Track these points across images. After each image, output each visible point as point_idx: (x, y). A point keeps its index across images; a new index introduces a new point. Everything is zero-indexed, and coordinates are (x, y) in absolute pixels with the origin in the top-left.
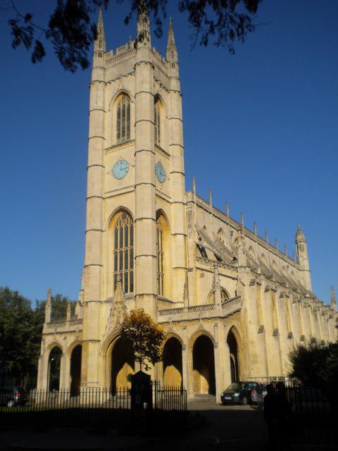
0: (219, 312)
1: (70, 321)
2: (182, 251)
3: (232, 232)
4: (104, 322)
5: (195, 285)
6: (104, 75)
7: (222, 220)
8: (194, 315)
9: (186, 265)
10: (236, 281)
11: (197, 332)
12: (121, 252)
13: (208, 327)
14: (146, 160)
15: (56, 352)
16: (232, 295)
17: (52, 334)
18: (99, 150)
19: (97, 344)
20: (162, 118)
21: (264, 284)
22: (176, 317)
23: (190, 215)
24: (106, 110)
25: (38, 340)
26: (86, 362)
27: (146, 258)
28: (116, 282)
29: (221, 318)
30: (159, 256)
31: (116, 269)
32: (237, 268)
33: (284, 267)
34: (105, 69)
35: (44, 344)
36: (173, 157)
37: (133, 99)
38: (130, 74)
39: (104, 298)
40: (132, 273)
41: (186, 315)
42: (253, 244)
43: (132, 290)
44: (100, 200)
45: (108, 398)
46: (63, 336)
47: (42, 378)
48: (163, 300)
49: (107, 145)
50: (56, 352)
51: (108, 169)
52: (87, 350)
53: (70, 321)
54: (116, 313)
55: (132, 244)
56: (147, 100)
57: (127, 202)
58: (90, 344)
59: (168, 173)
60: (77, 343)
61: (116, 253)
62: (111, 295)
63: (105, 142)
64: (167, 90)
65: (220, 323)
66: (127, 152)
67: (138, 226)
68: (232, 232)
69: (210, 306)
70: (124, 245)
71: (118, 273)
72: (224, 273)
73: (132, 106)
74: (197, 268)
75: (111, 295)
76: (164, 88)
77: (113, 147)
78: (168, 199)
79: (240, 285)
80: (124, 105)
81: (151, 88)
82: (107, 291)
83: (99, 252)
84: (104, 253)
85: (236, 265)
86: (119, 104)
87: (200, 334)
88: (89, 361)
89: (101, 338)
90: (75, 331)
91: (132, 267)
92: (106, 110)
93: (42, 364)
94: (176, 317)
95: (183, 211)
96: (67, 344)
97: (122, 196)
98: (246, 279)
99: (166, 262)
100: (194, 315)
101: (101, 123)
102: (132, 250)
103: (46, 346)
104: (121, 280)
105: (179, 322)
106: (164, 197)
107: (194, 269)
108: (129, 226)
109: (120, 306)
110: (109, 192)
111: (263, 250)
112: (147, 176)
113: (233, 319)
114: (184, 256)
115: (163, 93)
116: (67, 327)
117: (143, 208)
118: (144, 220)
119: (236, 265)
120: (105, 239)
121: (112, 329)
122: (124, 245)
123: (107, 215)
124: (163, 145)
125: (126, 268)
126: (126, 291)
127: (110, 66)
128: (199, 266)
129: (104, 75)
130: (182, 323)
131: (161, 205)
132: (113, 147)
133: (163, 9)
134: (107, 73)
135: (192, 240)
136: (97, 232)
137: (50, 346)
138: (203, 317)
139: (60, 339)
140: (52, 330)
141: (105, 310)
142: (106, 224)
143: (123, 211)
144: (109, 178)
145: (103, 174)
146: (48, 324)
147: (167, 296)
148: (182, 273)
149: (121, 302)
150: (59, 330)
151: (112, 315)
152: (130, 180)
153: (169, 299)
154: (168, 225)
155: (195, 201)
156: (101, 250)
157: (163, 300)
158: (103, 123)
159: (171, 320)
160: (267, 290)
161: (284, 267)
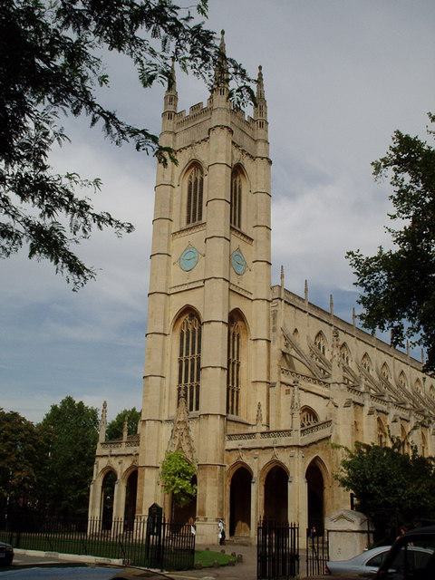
0: (297, 438)
2: (264, 360)
4: (164, 446)
5: (279, 404)
6: (175, 141)
8: (267, 442)
9: (269, 378)
10: (327, 401)
11: (270, 463)
13: (283, 457)
14: (218, 248)
15: (110, 478)
16: (322, 418)
17: (107, 456)
18: (164, 234)
19: (155, 472)
20: (244, 192)
21: (368, 404)
22: (247, 443)
25: (91, 461)
26: (142, 491)
28: (179, 397)
29: (299, 446)
30: (232, 368)
31: (180, 382)
33: (418, 380)
37: (205, 172)
38: (205, 140)
39: (165, 417)
40: (198, 387)
41: (260, 442)
42: (369, 350)
43: (197, 409)
44: (163, 296)
46: (120, 459)
48: (236, 422)
49: (175, 228)
50: (110, 478)
51: (174, 257)
52: (143, 477)
55: (199, 352)
57: (192, 299)
58: (147, 470)
59: (249, 262)
60: (133, 469)
62: (173, 413)
63: (173, 224)
64: (252, 157)
65: (298, 454)
66: (196, 237)
69: (287, 432)
70: (194, 407)
71: (183, 387)
73: (205, 179)
75: (173, 413)
76: (248, 154)
78: (249, 296)
79: (331, 406)
81: (227, 159)
82: (169, 408)
83: (160, 360)
84: (167, 361)
85: (329, 381)
86: (191, 177)
87: (239, 466)
88: (145, 492)
89: (160, 465)
90: (131, 455)
91: (198, 380)
92: (175, 185)
94: (247, 443)
96: (121, 468)
98: (341, 396)
99: (243, 375)
100: (267, 442)
102: (199, 358)
104: (186, 395)
105: (250, 449)
106: (246, 295)
109: (183, 427)
111: (385, 358)
112: (218, 269)
113: (317, 448)
114: (266, 368)
115: (247, 163)
116: (123, 449)
117: (214, 309)
119: (329, 381)
120: (168, 345)
122: (194, 407)
123: (172, 315)
124: (243, 229)
125: (192, 380)
126: (191, 410)
128: (284, 380)
129: (175, 141)
130: (252, 451)
131: (237, 303)
133: (249, 80)
135: (278, 346)
139: (115, 463)
140: (106, 452)
141: (166, 430)
142: (169, 329)
143: (189, 311)
144: (175, 270)
147: (242, 417)
148: (264, 387)
150: (115, 452)
151: (173, 437)
152: (198, 274)
154: (246, 328)
156: (163, 358)
157: (236, 422)
159: (241, 447)
160: (370, 413)
161: (418, 380)
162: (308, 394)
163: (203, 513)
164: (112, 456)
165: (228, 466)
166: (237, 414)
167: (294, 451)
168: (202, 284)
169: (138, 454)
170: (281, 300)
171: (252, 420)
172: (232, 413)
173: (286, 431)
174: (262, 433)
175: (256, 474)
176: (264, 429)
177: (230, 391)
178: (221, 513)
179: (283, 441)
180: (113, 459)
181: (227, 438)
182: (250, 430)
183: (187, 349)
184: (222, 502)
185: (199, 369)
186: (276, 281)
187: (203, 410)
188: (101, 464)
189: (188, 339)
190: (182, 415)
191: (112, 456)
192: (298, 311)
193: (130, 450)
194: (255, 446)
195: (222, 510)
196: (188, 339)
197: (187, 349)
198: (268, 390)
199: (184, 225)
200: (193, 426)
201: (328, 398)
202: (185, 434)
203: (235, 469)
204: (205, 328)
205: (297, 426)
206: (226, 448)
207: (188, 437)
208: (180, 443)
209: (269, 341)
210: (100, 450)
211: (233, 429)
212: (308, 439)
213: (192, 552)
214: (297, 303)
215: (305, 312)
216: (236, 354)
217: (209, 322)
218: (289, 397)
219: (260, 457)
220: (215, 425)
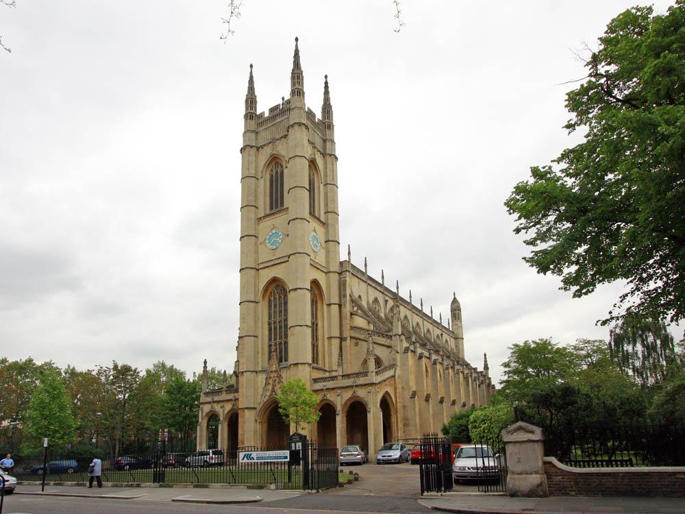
3: (387, 301)
10: (389, 350)
22: (330, 384)
28: (270, 352)
35: (202, 411)
43: (286, 360)
52: (243, 416)
53: (226, 391)
68: (387, 301)
77: (266, 216)
80: (277, 171)
85: (390, 334)
86: (272, 171)
87: (323, 403)
93: (201, 430)
105: (333, 389)
110: (262, 263)
118: (298, 290)
121: (267, 397)
123: (262, 286)
126: (281, 361)
132: (266, 216)
136: (251, 304)
138: (357, 384)
140: (209, 399)
149: (276, 371)
150: (216, 398)
164: (214, 402)
168: (286, 259)
175: (339, 408)
180: (215, 405)
182: (334, 374)
190: (274, 366)
191: (214, 402)
193: (231, 396)
197: (280, 333)
199: (268, 212)
202: (277, 380)
208: (273, 388)
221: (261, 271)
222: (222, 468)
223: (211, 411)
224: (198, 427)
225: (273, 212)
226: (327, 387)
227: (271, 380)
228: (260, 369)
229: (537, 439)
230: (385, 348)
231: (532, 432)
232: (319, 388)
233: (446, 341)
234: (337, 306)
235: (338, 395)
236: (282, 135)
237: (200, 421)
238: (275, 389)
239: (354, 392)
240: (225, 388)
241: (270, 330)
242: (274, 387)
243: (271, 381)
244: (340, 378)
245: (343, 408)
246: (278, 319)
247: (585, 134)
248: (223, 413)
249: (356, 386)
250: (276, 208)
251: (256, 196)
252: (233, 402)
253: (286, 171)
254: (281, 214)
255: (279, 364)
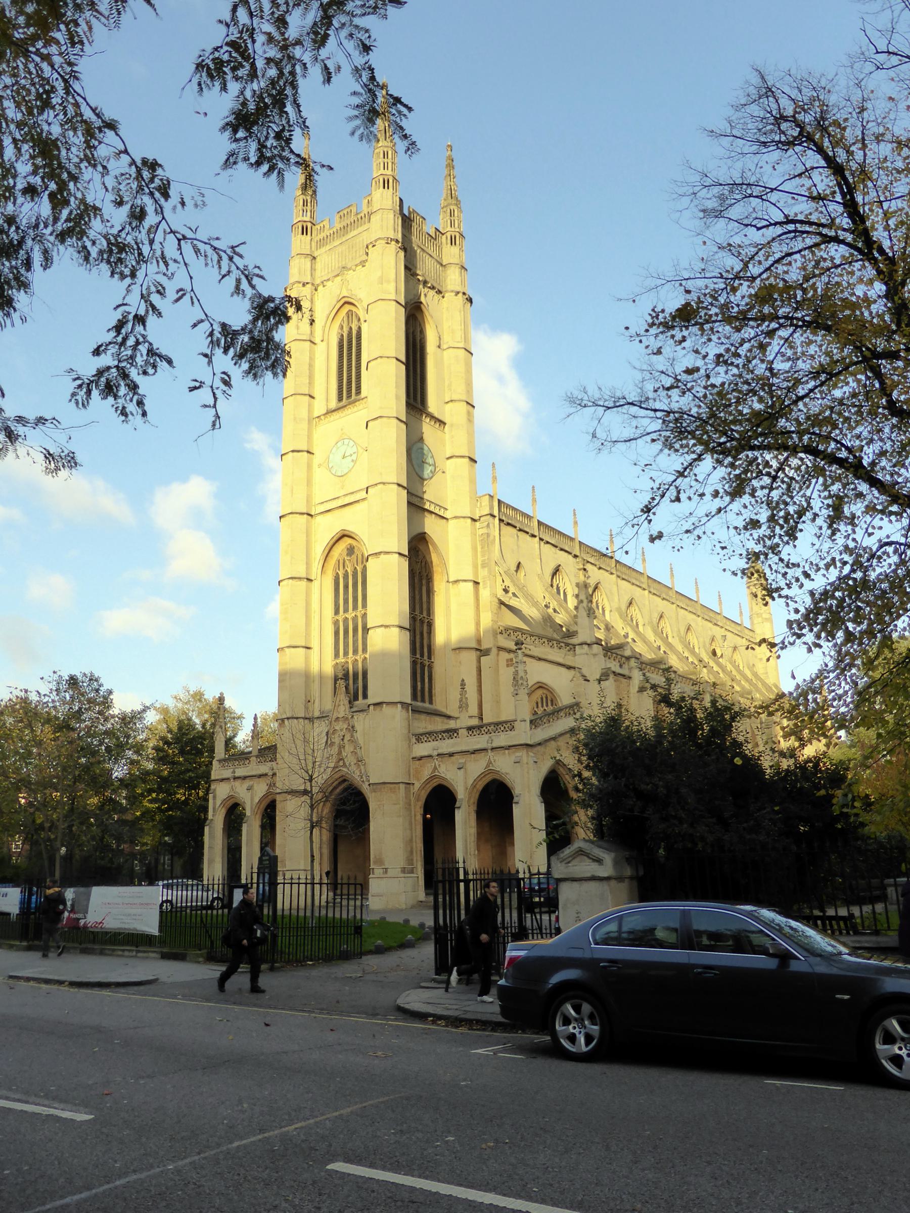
0: (523, 734)
1: (257, 757)
6: (313, 269)
7: (562, 550)
8: (480, 741)
10: (572, 672)
12: (346, 620)
22: (446, 746)
23: (487, 539)
24: (317, 340)
27: (387, 630)
32: (574, 646)
34: (314, 258)
35: (214, 798)
36: (452, 425)
43: (365, 696)
45: (324, 897)
46: (247, 783)
47: (211, 862)
49: (319, 407)
53: (257, 757)
54: (337, 740)
55: (364, 605)
56: (146, 242)
60: (270, 798)
61: (336, 623)
66: (355, 415)
67: (373, 566)
69: (507, 725)
72: (550, 657)
74: (500, 649)
76: (433, 288)
77: (329, 412)
80: (351, 328)
85: (574, 641)
86: (342, 327)
87: (488, 779)
93: (212, 836)
95: (474, 534)
97: (347, 508)
101: (307, 367)
102: (364, 616)
103: (218, 802)
105: (451, 755)
107: (463, 732)
108: (359, 569)
118: (382, 556)
119: (574, 641)
123: (318, 550)
126: (356, 698)
127: (323, 250)
129: (313, 269)
130: (456, 757)
132: (329, 412)
134: (319, 265)
136: (299, 583)
137: (224, 801)
138: (495, 745)
140: (227, 773)
145: (309, 466)
146: (220, 761)
148: (473, 655)
149: (345, 719)
150: (240, 772)
153: (444, 710)
155: (496, 513)
157: (428, 713)
158: (311, 366)
160: (642, 690)
162: (542, 663)
163: (380, 862)
164: (235, 778)
165: (417, 785)
166: (431, 702)
167: (522, 754)
168: (363, 494)
169: (274, 774)
170: (494, 517)
171: (452, 710)
172: (423, 701)
173: (506, 722)
174: (470, 729)
175: (461, 794)
176: (475, 722)
177: (418, 666)
178: (410, 861)
179: (502, 739)
180: (237, 784)
181: (414, 740)
182: (452, 724)
183: (346, 601)
184: (411, 840)
185: (366, 630)
186: (485, 487)
187: (371, 699)
188: (220, 793)
189: (346, 587)
190: (342, 708)
191: (235, 778)
192: (521, 534)
193: (264, 768)
194: (459, 749)
195: (411, 852)
196: (346, 587)
197: (346, 601)
198: (479, 661)
199: (333, 403)
200: (361, 722)
201: (574, 668)
202: (347, 737)
203: (429, 788)
204: (372, 564)
205: (526, 713)
206: (414, 756)
207: (353, 741)
208: (340, 753)
209: (476, 583)
210: (217, 771)
211: (425, 724)
212: (541, 734)
213: (358, 930)
214: (519, 520)
215: (533, 536)
216: (425, 606)
217: (377, 554)
218: (512, 669)
219: (255, 787)
220: (396, 718)
221: (319, 519)
222: (344, 916)
223: (231, 797)
224: (206, 829)
225: (341, 404)
226: (440, 751)
227: (336, 736)
228: (317, 714)
229: (605, 875)
230: (563, 670)
231: (599, 861)
232: (426, 754)
233: (665, 652)
234: (471, 584)
235: (459, 769)
236: (358, 261)
237: (210, 816)
238: (344, 754)
239: (435, 768)
240: (255, 753)
241: (337, 633)
242: (341, 747)
243: (337, 740)
244: (463, 732)
245: (470, 793)
246: (350, 615)
247: (110, 274)
248: (252, 799)
249: (492, 749)
250: (349, 396)
251: (311, 377)
252: (268, 780)
253: (364, 327)
254: (356, 409)
255: (350, 702)
